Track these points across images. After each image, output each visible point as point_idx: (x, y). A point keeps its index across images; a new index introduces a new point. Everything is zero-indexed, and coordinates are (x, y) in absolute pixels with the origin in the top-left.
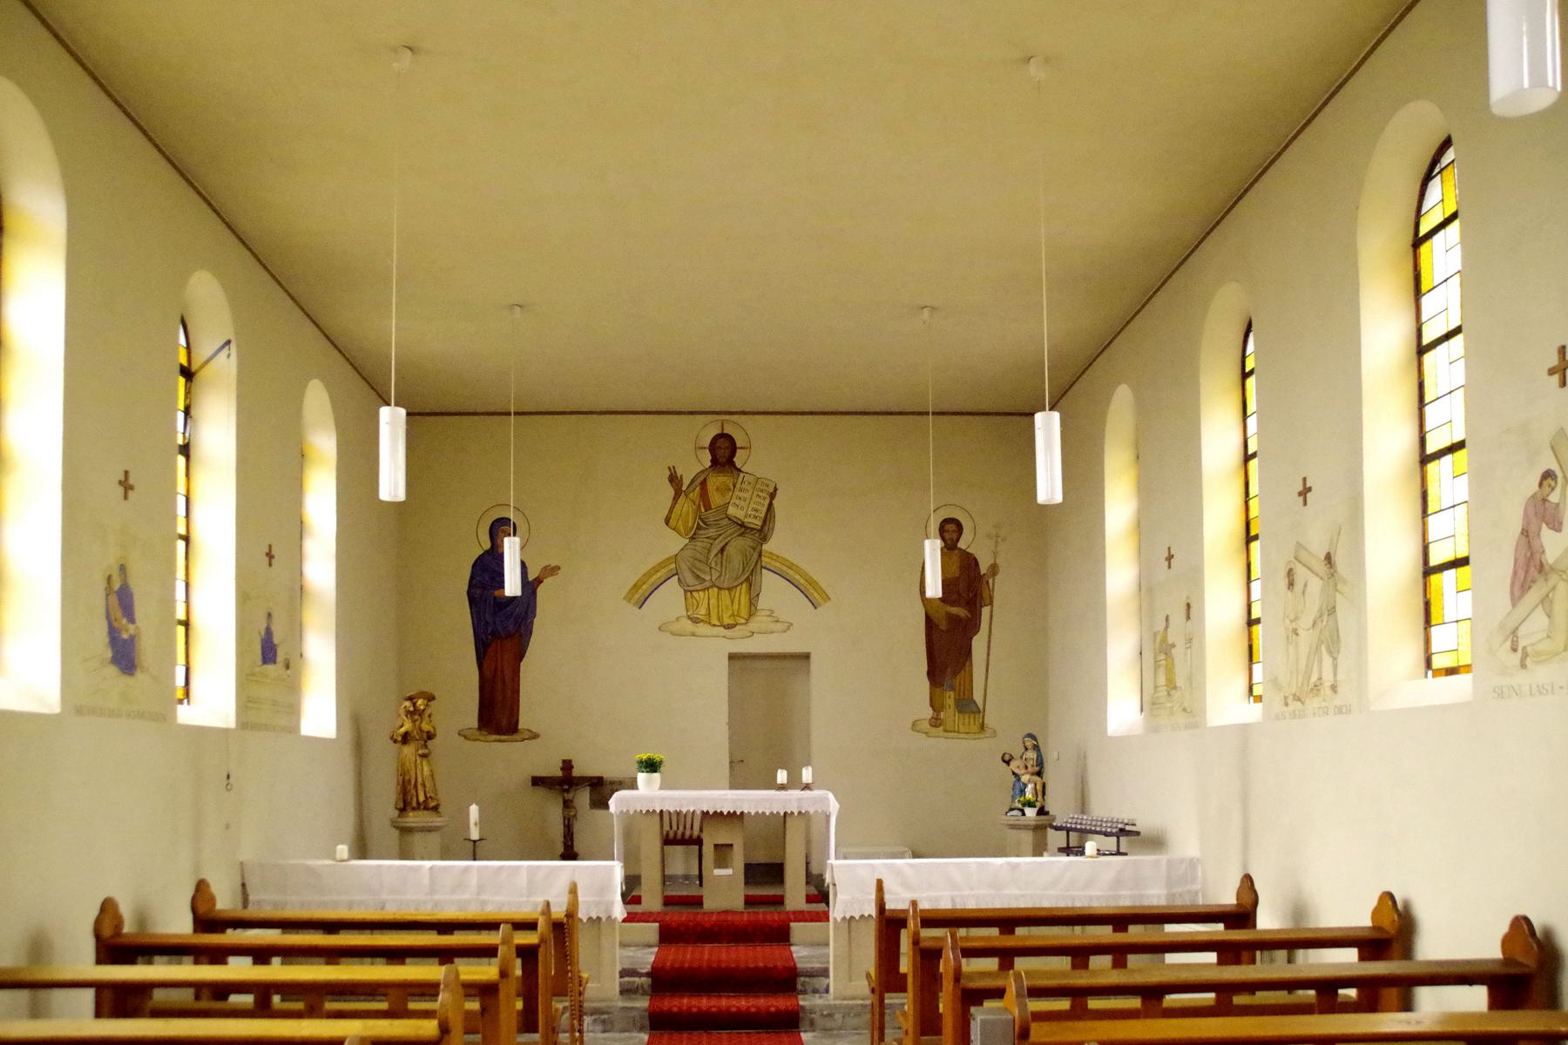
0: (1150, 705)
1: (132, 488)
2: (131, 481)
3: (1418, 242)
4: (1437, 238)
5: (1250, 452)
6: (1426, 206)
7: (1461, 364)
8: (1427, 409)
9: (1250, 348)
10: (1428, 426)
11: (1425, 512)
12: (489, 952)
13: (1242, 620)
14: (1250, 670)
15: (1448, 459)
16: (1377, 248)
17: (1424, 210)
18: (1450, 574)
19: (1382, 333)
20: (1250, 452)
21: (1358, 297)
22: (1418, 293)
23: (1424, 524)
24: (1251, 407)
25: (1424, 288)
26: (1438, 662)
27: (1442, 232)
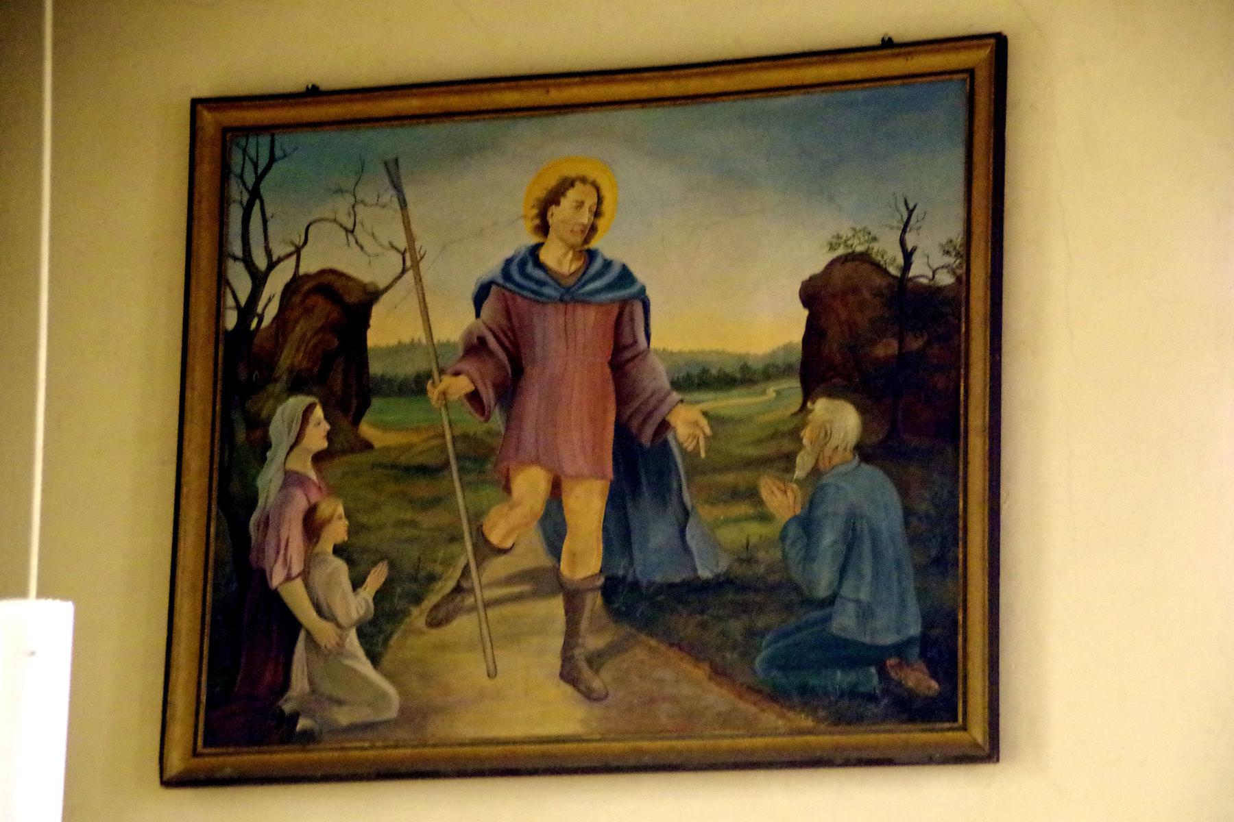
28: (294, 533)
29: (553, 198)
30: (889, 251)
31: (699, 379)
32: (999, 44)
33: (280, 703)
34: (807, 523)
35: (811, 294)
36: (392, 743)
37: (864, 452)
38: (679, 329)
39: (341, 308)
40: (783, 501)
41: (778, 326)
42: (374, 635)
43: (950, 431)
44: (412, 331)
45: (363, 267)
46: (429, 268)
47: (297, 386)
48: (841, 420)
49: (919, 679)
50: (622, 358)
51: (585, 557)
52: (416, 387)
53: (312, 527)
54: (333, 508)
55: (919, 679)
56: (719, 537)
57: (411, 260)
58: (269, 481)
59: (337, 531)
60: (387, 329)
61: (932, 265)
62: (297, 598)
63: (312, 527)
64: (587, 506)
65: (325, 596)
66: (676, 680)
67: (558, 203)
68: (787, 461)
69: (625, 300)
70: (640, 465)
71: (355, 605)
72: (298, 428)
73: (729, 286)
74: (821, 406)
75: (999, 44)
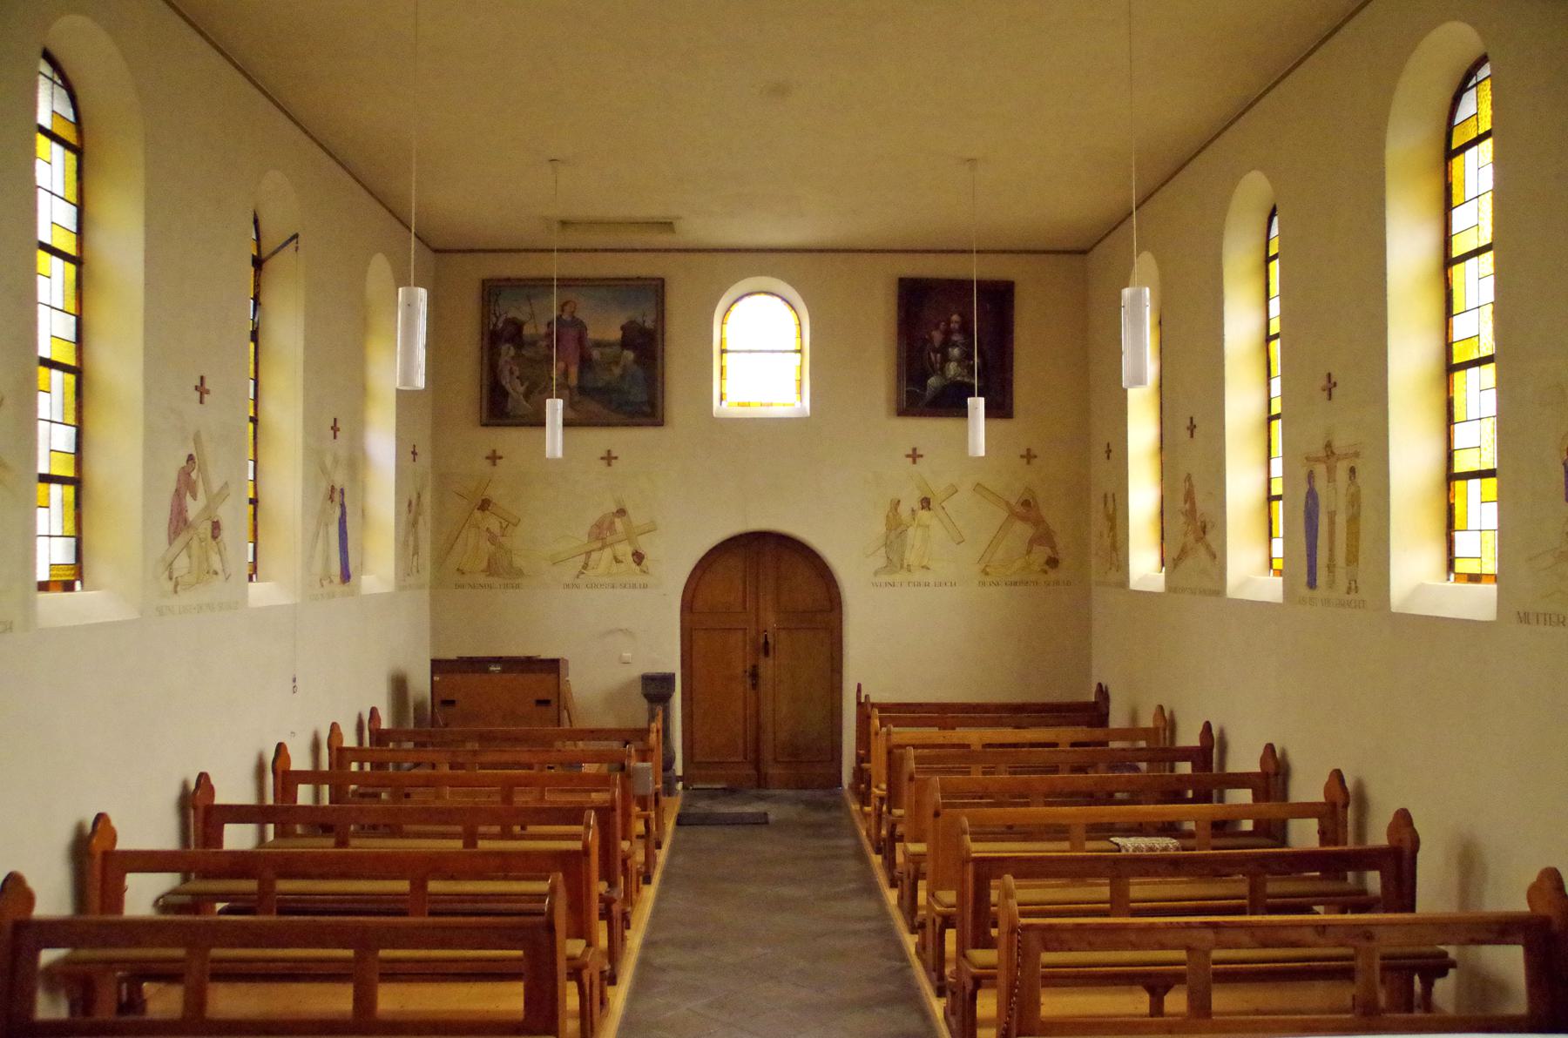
0: (1171, 560)
1: (208, 392)
2: (207, 386)
3: (1450, 154)
4: (1471, 153)
5: (1271, 254)
6: (1460, 116)
7: (1491, 281)
8: (1457, 428)
9: (1275, 231)
10: (1455, 228)
11: (1450, 420)
12: (574, 815)
13: (1260, 337)
14: (1269, 384)
15: (1473, 261)
16: (1405, 147)
17: (1457, 120)
18: (1474, 483)
19: (1407, 248)
20: (1271, 254)
21: (1384, 213)
22: (1448, 207)
23: (1447, 173)
24: (1275, 289)
25: (1455, 202)
26: (1460, 566)
27: (1475, 259)
28: (507, 373)
29: (566, 304)
30: (640, 320)
31: (598, 344)
32: (662, 280)
33: (350, 1015)
34: (622, 377)
35: (623, 328)
36: (969, 987)
37: (636, 361)
38: (592, 335)
39: (518, 326)
40: (617, 371)
41: (615, 334)
42: (527, 395)
43: (654, 358)
44: (533, 331)
45: (521, 317)
46: (539, 318)
47: (507, 341)
48: (629, 355)
49: (646, 409)
50: (581, 338)
51: (573, 380)
52: (534, 343)
53: (512, 373)
54: (516, 368)
55: (646, 409)
56: (602, 378)
57: (532, 315)
58: (501, 362)
59: (517, 373)
60: (528, 330)
61: (649, 324)
62: (508, 387)
63: (512, 373)
64: (574, 370)
65: (516, 388)
66: (593, 407)
67: (506, 394)
68: (617, 363)
69: (581, 327)
70: (585, 362)
71: (522, 389)
72: (507, 351)
73: (606, 327)
74: (626, 352)
75: (662, 280)
